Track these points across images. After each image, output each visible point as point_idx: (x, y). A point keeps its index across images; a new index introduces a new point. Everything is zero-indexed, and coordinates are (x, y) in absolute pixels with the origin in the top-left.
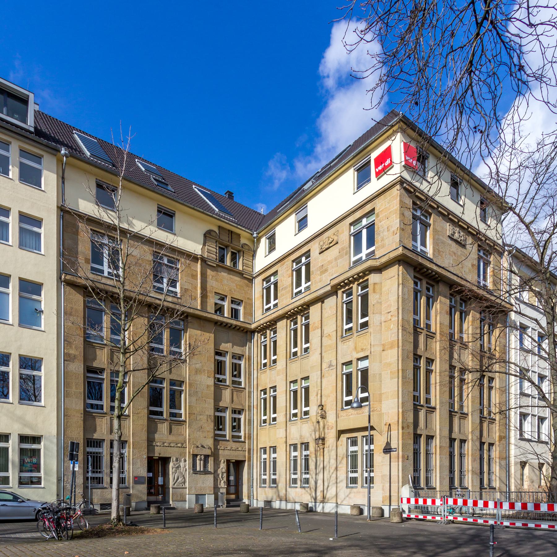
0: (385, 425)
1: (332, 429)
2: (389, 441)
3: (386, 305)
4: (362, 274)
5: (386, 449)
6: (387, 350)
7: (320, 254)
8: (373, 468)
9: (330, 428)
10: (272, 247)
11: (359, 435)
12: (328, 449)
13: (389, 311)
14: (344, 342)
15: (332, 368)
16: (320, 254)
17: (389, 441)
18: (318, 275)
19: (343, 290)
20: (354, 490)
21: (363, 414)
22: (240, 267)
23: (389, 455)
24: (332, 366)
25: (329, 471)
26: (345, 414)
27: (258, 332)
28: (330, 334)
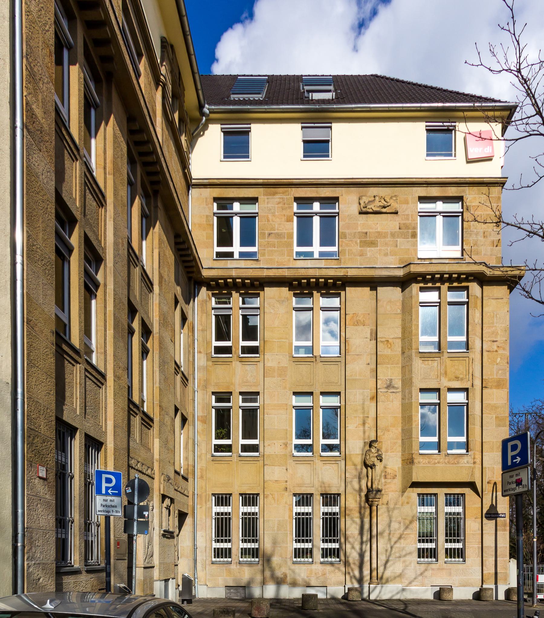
0: (488, 483)
1: (394, 477)
2: (494, 503)
3: (490, 331)
4: (249, 281)
5: (491, 514)
6: (491, 388)
8: (229, 536)
9: (388, 477)
11: (441, 492)
12: (384, 506)
13: (495, 339)
14: (423, 359)
17: (494, 503)
19: (422, 285)
20: (433, 566)
21: (459, 465)
23: (494, 521)
24: (393, 387)
25: (390, 540)
27: (209, 288)
28: (390, 340)
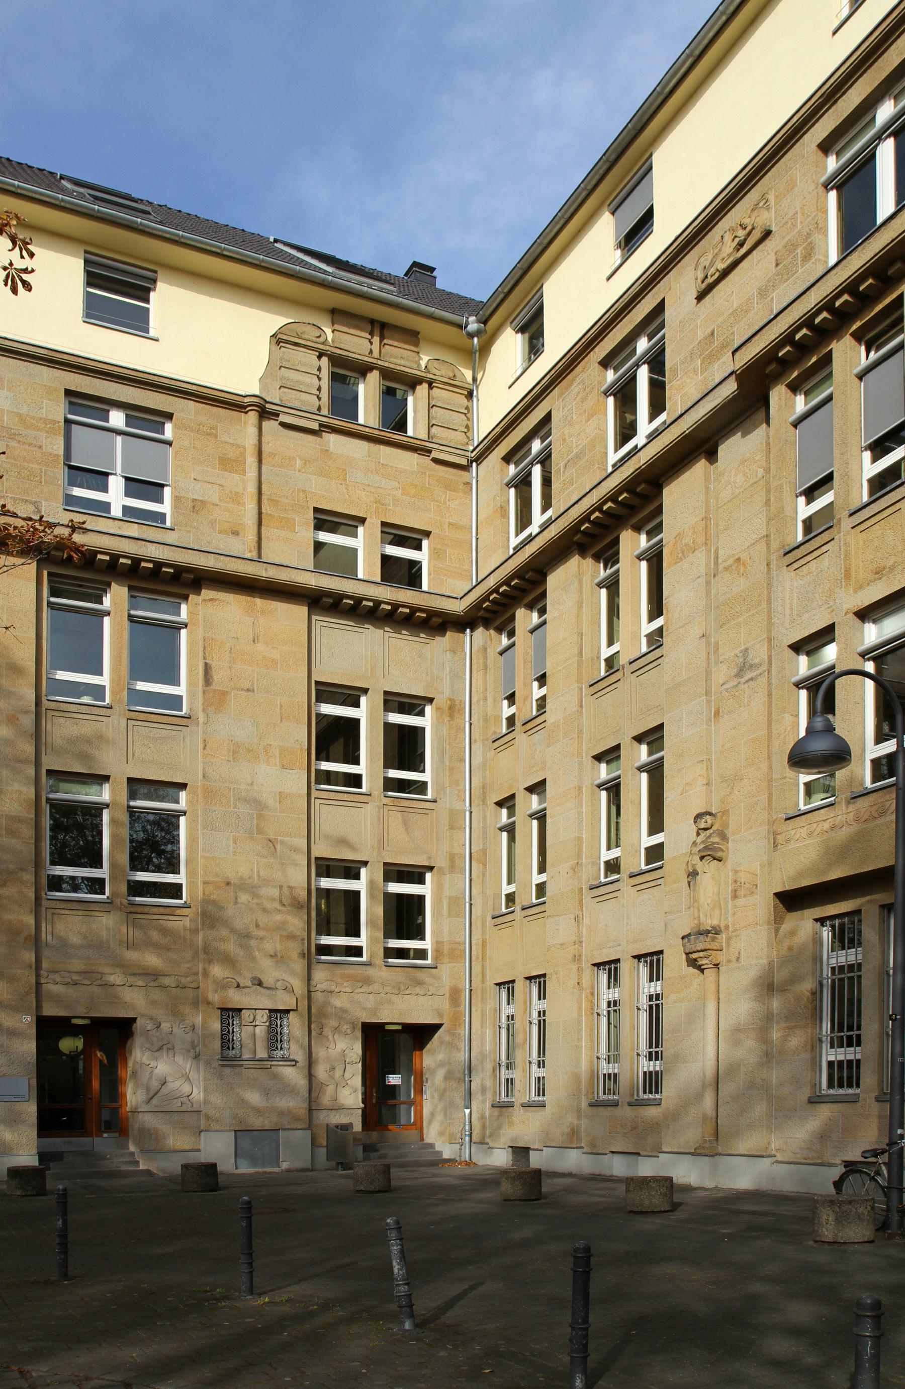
7: (700, 297)
10: (535, 348)
14: (796, 566)
15: (753, 674)
16: (700, 297)
18: (695, 371)
22: (415, 427)
26: (804, 832)
28: (743, 556)
